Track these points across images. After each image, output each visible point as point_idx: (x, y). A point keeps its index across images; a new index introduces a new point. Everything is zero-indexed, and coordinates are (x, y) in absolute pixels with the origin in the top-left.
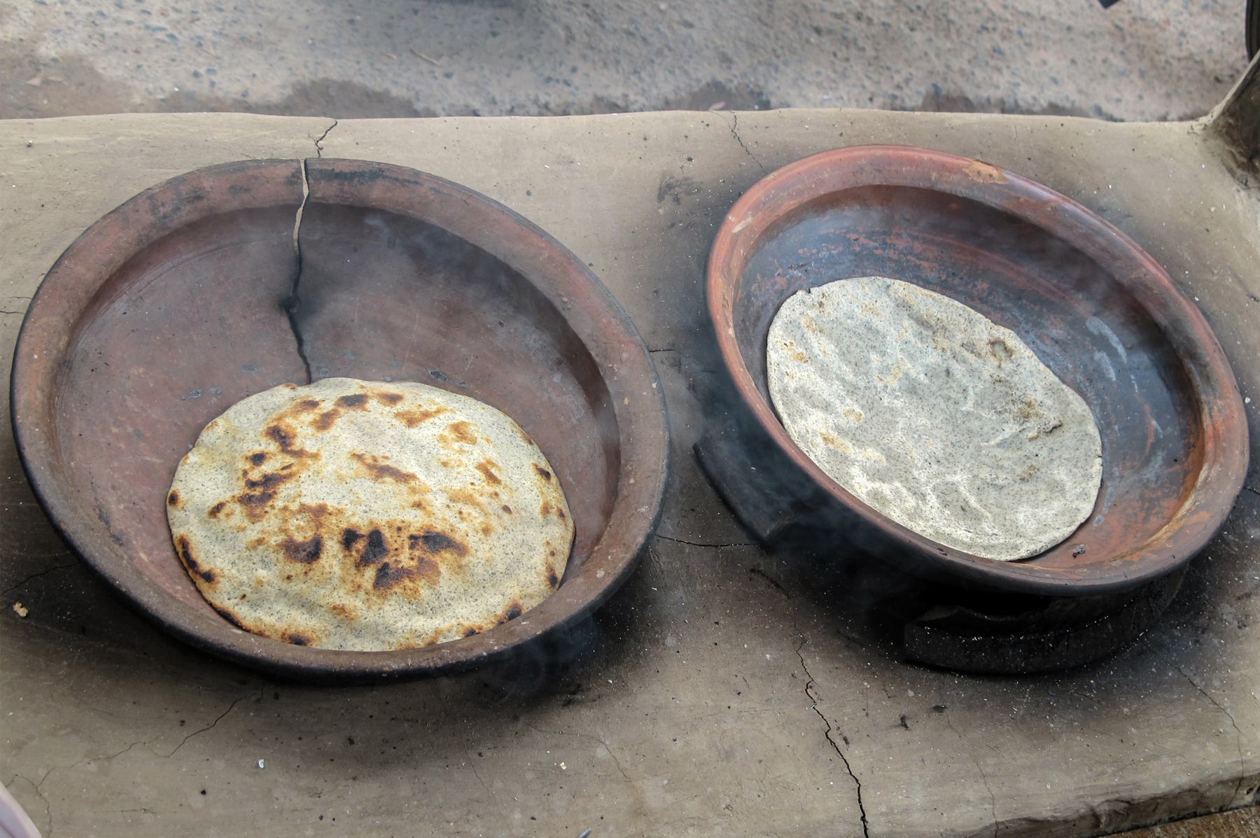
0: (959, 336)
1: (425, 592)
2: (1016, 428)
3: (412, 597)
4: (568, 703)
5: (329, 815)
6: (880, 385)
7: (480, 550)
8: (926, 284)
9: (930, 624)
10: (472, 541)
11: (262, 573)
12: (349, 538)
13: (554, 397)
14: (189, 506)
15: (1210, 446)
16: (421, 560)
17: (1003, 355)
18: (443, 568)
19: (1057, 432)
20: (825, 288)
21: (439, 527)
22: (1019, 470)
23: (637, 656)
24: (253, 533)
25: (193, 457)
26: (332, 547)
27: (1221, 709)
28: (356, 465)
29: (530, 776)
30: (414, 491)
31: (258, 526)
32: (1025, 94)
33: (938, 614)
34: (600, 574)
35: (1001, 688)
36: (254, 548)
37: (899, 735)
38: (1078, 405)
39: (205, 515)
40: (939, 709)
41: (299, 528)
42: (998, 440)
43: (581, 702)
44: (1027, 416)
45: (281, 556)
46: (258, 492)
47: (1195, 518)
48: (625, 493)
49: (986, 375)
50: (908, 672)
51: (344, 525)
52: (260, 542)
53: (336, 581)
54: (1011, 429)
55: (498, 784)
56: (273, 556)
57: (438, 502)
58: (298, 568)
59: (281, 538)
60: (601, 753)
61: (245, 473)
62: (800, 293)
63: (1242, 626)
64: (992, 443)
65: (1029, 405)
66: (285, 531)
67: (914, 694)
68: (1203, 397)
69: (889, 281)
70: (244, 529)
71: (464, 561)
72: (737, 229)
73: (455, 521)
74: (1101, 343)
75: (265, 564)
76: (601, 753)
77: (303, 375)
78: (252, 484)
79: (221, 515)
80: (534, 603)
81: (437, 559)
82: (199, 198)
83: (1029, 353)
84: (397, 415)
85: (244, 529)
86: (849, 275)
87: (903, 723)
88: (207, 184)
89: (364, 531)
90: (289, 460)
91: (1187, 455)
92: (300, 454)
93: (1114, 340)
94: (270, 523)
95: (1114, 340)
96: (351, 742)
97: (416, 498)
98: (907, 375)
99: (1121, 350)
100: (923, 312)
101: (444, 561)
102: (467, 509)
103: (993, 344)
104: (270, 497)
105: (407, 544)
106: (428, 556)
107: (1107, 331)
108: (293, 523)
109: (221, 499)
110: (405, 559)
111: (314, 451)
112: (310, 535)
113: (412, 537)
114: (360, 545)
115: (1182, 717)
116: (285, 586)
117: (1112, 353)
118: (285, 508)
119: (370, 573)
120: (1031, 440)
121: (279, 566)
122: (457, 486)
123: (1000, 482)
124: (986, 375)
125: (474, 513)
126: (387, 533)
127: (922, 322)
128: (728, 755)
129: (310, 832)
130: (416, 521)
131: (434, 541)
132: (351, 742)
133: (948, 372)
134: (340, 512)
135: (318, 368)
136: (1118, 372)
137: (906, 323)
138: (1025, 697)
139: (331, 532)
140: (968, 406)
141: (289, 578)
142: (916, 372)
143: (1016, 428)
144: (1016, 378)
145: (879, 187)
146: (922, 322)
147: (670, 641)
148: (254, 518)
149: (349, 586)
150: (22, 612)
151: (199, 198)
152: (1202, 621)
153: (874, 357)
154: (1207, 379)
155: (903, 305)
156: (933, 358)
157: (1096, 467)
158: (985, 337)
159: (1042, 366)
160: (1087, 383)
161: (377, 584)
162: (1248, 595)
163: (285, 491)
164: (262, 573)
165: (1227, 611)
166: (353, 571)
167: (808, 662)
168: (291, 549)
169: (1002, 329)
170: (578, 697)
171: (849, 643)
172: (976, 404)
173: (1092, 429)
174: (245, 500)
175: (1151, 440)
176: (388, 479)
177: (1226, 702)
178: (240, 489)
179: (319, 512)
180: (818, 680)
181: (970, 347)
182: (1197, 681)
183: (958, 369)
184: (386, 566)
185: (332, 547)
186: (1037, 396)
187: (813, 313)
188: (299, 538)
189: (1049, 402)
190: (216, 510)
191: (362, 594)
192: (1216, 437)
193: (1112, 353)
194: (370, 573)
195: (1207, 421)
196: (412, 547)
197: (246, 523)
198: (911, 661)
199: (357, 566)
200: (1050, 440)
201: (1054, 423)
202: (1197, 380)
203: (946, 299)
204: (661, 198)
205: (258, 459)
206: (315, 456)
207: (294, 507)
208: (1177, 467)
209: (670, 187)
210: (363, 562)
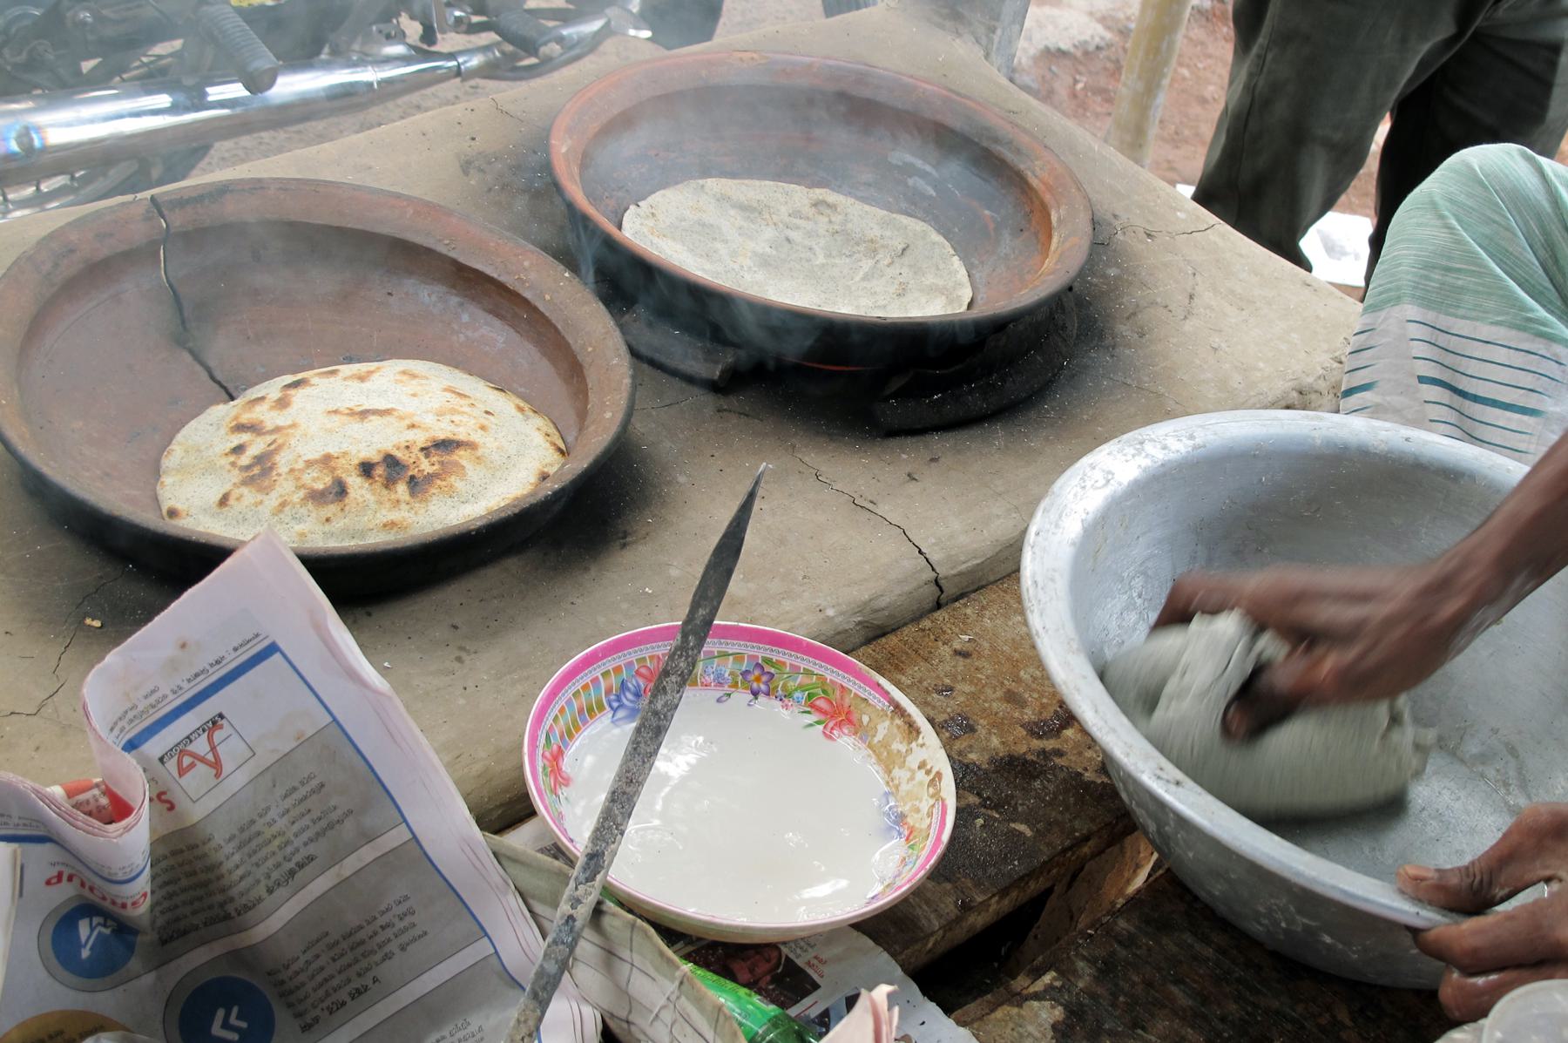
0: (783, 209)
1: (459, 485)
2: (871, 262)
3: (451, 492)
4: (624, 546)
5: (470, 684)
6: (736, 267)
7: (487, 442)
8: (733, 175)
9: (895, 395)
10: (476, 437)
11: (299, 528)
12: (366, 469)
13: (469, 333)
14: (192, 511)
15: (1047, 198)
16: (442, 463)
17: (829, 211)
18: (464, 462)
19: (908, 252)
20: (650, 199)
21: (442, 436)
22: (892, 290)
23: (660, 496)
24: (272, 500)
25: (167, 480)
26: (355, 482)
27: (1159, 396)
28: (336, 418)
29: (625, 606)
30: (401, 418)
31: (274, 494)
32: (314, 797)
33: (896, 383)
34: (608, 415)
35: (976, 432)
36: (281, 511)
37: (912, 487)
38: (916, 226)
39: (216, 509)
40: (933, 460)
41: (314, 480)
42: (861, 273)
43: (635, 542)
44: (875, 251)
45: (310, 506)
46: (256, 470)
47: (1067, 245)
48: (588, 360)
49: (822, 232)
50: (894, 443)
51: (356, 462)
52: (283, 504)
53: (373, 506)
54: (866, 265)
55: (601, 620)
56: (303, 511)
57: (429, 420)
58: (331, 509)
59: (302, 493)
60: (674, 572)
61: (233, 464)
62: (632, 207)
63: (1142, 335)
64: (857, 279)
65: (872, 241)
66: (303, 486)
67: (908, 455)
68: (1022, 167)
69: (701, 182)
70: (261, 502)
71: (479, 452)
72: (564, 150)
73: (452, 428)
74: (909, 170)
75: (299, 520)
76: (674, 572)
77: (226, 396)
78: (248, 468)
79: (232, 501)
80: (555, 468)
81: (455, 457)
82: (72, 251)
83: (851, 200)
84: (345, 379)
85: (261, 502)
86: (664, 185)
87: (911, 477)
88: (74, 237)
89: (376, 458)
90: (269, 439)
91: (1030, 221)
92: (277, 429)
93: (919, 163)
94: (285, 487)
95: (919, 163)
96: (455, 627)
97: (408, 422)
98: (755, 253)
99: (928, 168)
100: (742, 198)
101: (461, 456)
102: (456, 418)
103: (815, 205)
104: (271, 468)
105: (421, 455)
106: (446, 458)
107: (909, 158)
108: (307, 478)
109: (223, 491)
110: (426, 466)
111: (289, 422)
112: (328, 480)
113: (422, 449)
114: (379, 471)
115: (1132, 410)
116: (327, 528)
117: (924, 175)
118: (292, 470)
119: (402, 489)
120: (888, 266)
121: (314, 515)
122: (436, 406)
123: (881, 303)
124: (822, 232)
125: (465, 419)
126: (399, 454)
127: (744, 208)
128: (782, 542)
129: (462, 701)
130: (420, 438)
131: (445, 445)
132: (455, 627)
133: (788, 240)
134: (345, 453)
135: (237, 388)
136: (935, 188)
137: (732, 212)
138: (999, 434)
139: (347, 471)
140: (821, 259)
141: (328, 520)
142: (763, 247)
143: (871, 262)
144: (850, 226)
145: (659, 97)
146: (744, 208)
147: (682, 479)
148: (266, 491)
149: (388, 505)
150: (97, 624)
151: (72, 251)
152: (1108, 341)
153: (718, 245)
154: (1018, 151)
155: (722, 199)
156: (769, 233)
157: (956, 262)
158: (806, 202)
159: (867, 208)
160: (915, 205)
161: (413, 494)
162: (1134, 314)
163: (283, 461)
164: (299, 528)
165: (1123, 329)
166: (385, 492)
167: (806, 459)
168: (317, 497)
169: (818, 191)
170: (629, 539)
171: (831, 437)
172: (828, 256)
173: (936, 237)
174: (248, 482)
175: (992, 226)
176: (372, 418)
177: (1161, 389)
178: (236, 476)
179: (327, 460)
180: (823, 469)
181: (796, 214)
182: (1129, 381)
183: (793, 235)
184: (412, 477)
185: (355, 482)
186: (875, 232)
187: (651, 223)
188: (320, 486)
189: (888, 233)
190: (224, 501)
191: (403, 506)
192: (1050, 188)
193: (924, 175)
194: (402, 489)
195: (1034, 182)
196: (427, 456)
197: (260, 497)
198: (892, 433)
199: (387, 487)
200: (906, 260)
201: (900, 247)
202: (1009, 156)
203: (757, 183)
204: (466, 173)
205: (239, 450)
206: (294, 426)
207: (300, 465)
208: (1026, 234)
209: (469, 163)
210: (389, 483)
